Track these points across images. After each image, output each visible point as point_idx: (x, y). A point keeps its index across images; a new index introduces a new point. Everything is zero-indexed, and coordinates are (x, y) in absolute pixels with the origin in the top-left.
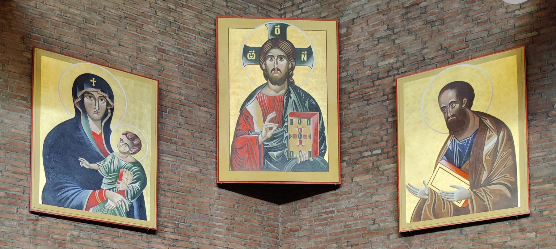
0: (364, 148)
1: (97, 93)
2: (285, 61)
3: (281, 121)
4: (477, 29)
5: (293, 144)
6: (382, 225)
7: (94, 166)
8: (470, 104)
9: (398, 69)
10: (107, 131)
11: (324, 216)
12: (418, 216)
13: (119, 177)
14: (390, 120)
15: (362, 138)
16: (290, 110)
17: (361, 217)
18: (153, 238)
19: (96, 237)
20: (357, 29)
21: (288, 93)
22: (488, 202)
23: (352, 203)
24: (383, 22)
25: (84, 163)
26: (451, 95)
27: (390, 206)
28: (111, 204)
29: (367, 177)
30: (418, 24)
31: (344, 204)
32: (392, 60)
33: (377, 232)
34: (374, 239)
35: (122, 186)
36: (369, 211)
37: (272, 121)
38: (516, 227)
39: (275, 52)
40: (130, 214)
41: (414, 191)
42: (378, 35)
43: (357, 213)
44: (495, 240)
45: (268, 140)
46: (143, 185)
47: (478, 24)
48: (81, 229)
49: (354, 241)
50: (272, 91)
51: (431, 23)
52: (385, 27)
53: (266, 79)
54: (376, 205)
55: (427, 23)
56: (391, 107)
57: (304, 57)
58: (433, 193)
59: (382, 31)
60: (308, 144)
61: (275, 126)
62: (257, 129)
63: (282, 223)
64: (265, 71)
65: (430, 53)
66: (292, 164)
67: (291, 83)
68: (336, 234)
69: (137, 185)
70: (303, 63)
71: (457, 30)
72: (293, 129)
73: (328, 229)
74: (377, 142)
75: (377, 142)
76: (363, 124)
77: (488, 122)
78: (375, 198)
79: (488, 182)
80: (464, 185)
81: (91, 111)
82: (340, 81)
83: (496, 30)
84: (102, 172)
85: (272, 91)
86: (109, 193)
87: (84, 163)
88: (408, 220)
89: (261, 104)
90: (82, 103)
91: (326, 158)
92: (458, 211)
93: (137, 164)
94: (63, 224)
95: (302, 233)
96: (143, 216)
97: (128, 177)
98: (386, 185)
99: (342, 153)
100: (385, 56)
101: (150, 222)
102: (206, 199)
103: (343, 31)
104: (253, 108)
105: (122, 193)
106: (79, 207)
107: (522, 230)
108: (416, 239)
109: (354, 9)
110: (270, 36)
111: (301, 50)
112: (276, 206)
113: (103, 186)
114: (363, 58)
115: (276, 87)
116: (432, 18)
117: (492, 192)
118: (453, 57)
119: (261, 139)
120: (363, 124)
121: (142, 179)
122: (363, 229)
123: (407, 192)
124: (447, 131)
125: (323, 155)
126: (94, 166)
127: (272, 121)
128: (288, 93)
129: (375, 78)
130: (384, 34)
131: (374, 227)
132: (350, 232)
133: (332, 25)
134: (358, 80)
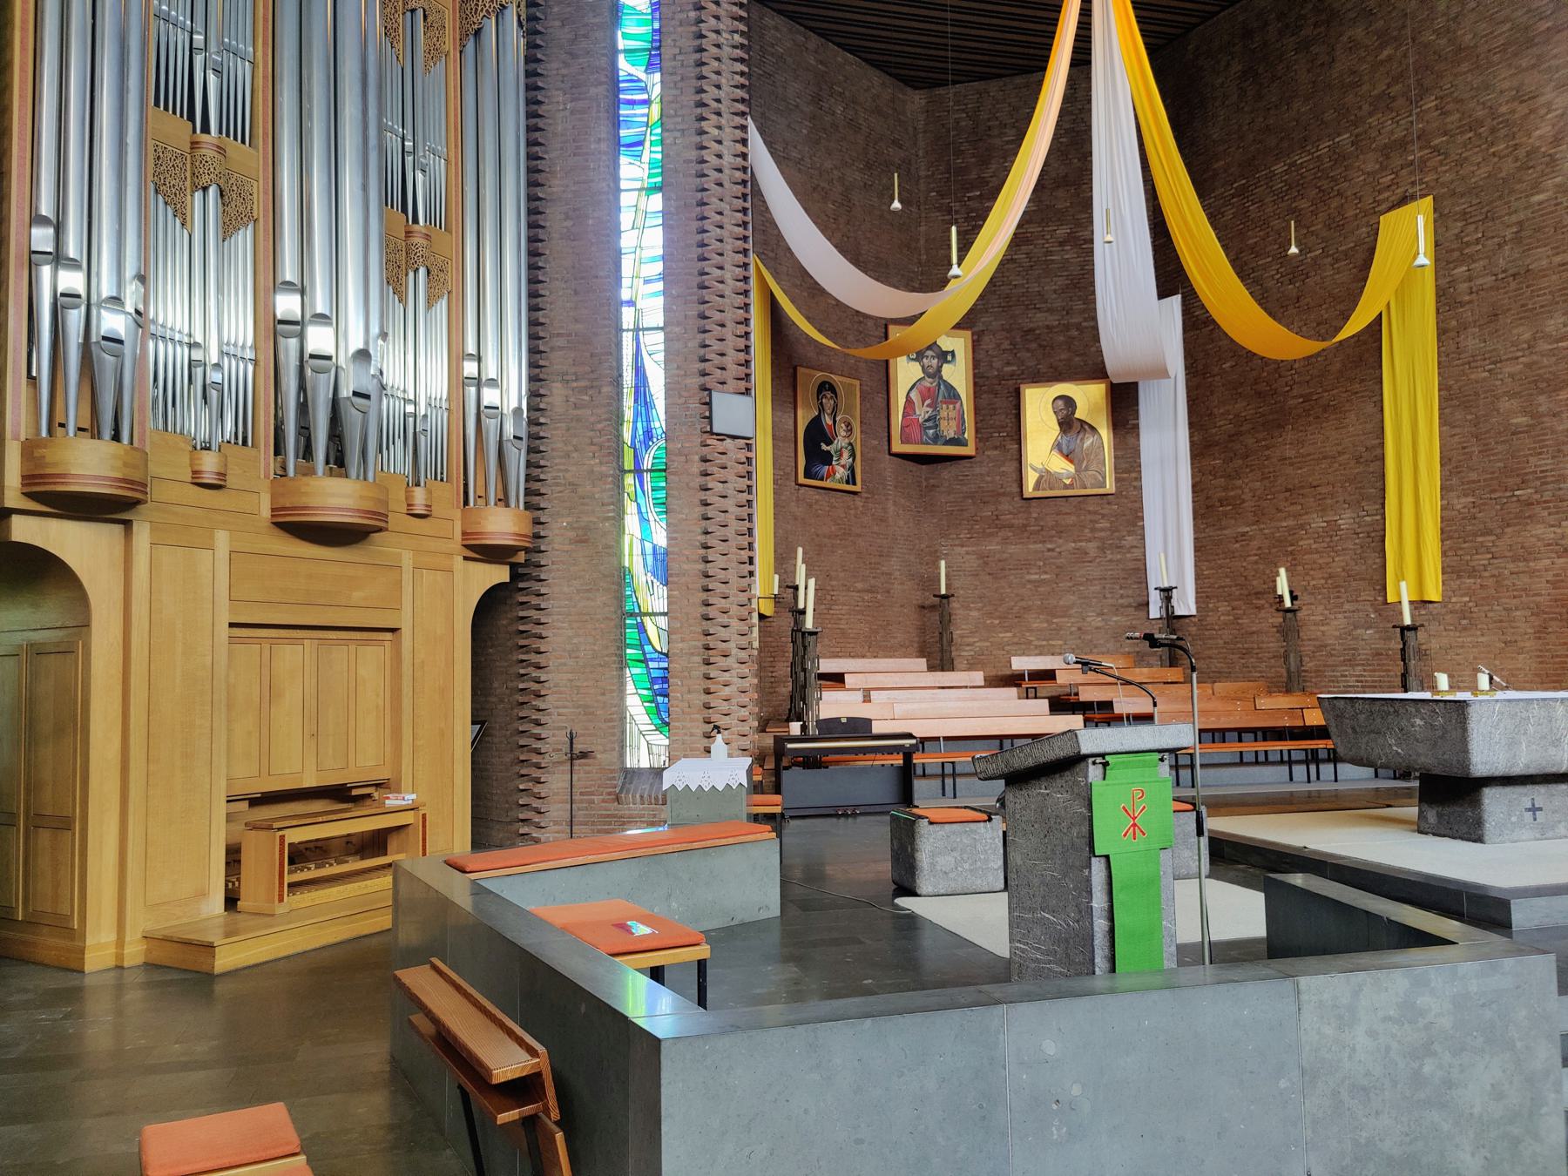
0: (992, 430)
1: (829, 394)
2: (936, 360)
3: (933, 405)
4: (1077, 359)
5: (943, 424)
6: (1008, 489)
7: (828, 448)
8: (1073, 413)
9: (1019, 375)
10: (835, 422)
11: (961, 478)
12: (1037, 486)
13: (841, 455)
14: (1014, 412)
15: (991, 422)
16: (940, 399)
17: (991, 482)
18: (856, 497)
19: (827, 499)
20: (986, 339)
21: (939, 385)
22: (1088, 484)
23: (984, 470)
24: (1007, 338)
25: (824, 447)
26: (1060, 403)
27: (1014, 476)
28: (838, 476)
29: (995, 452)
30: (1034, 346)
31: (978, 470)
32: (1015, 368)
33: (1004, 494)
34: (1002, 499)
35: (843, 462)
36: (998, 478)
37: (928, 406)
38: (1105, 501)
39: (929, 353)
40: (848, 482)
41: (1034, 469)
42: (1003, 347)
43: (989, 479)
44: (1091, 509)
45: (926, 421)
46: (854, 460)
47: (1078, 355)
48: (818, 493)
49: (986, 499)
50: (928, 383)
51: (1044, 347)
52: (1009, 342)
53: (924, 372)
54: (1003, 474)
55: (1040, 346)
56: (1014, 403)
57: (949, 358)
58: (1048, 471)
59: (1006, 345)
60: (953, 424)
61: (930, 410)
62: (918, 413)
63: (926, 480)
64: (923, 367)
65: (1043, 368)
66: (943, 440)
67: (941, 377)
68: (971, 492)
69: (851, 460)
70: (949, 362)
71: (1063, 357)
72: (944, 414)
73: (965, 489)
74: (1003, 427)
75: (1003, 427)
76: (992, 412)
77: (1086, 427)
78: (1002, 469)
79: (1087, 469)
80: (1071, 468)
81: (826, 408)
82: (975, 376)
83: (1090, 362)
84: (833, 452)
85: (928, 383)
86: (837, 468)
87: (824, 447)
88: (1030, 490)
89: (921, 392)
90: (821, 403)
91: (966, 436)
92: (1066, 487)
93: (850, 444)
94: (811, 492)
95: (943, 489)
96: (854, 484)
97: (846, 454)
98: (1011, 460)
99: (977, 431)
100: (1008, 364)
101: (857, 488)
102: (882, 465)
103: (976, 337)
104: (913, 395)
105: (843, 466)
106: (822, 479)
107: (1109, 503)
108: (1034, 503)
109: (983, 323)
110: (1473, 833)
111: (947, 352)
112: (920, 466)
113: (834, 463)
114: (992, 362)
115: (930, 380)
116: (1045, 343)
117: (1090, 476)
118: (1060, 374)
119: (921, 420)
120: (992, 412)
121: (853, 455)
122: (993, 491)
123: (1029, 468)
124: (1057, 428)
125: (964, 433)
126: (828, 448)
127: (928, 406)
128: (939, 385)
129: (1001, 378)
130: (1008, 347)
131: (1002, 490)
132: (983, 492)
133: (968, 333)
134: (988, 378)
